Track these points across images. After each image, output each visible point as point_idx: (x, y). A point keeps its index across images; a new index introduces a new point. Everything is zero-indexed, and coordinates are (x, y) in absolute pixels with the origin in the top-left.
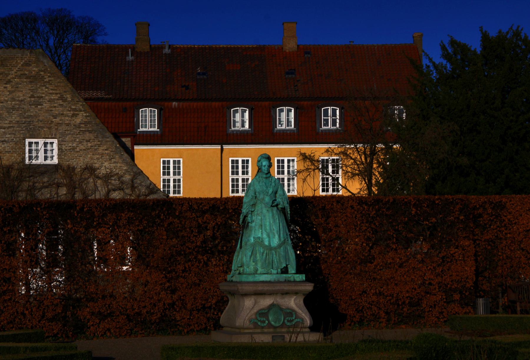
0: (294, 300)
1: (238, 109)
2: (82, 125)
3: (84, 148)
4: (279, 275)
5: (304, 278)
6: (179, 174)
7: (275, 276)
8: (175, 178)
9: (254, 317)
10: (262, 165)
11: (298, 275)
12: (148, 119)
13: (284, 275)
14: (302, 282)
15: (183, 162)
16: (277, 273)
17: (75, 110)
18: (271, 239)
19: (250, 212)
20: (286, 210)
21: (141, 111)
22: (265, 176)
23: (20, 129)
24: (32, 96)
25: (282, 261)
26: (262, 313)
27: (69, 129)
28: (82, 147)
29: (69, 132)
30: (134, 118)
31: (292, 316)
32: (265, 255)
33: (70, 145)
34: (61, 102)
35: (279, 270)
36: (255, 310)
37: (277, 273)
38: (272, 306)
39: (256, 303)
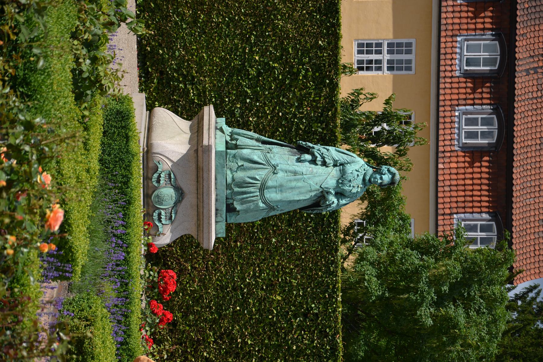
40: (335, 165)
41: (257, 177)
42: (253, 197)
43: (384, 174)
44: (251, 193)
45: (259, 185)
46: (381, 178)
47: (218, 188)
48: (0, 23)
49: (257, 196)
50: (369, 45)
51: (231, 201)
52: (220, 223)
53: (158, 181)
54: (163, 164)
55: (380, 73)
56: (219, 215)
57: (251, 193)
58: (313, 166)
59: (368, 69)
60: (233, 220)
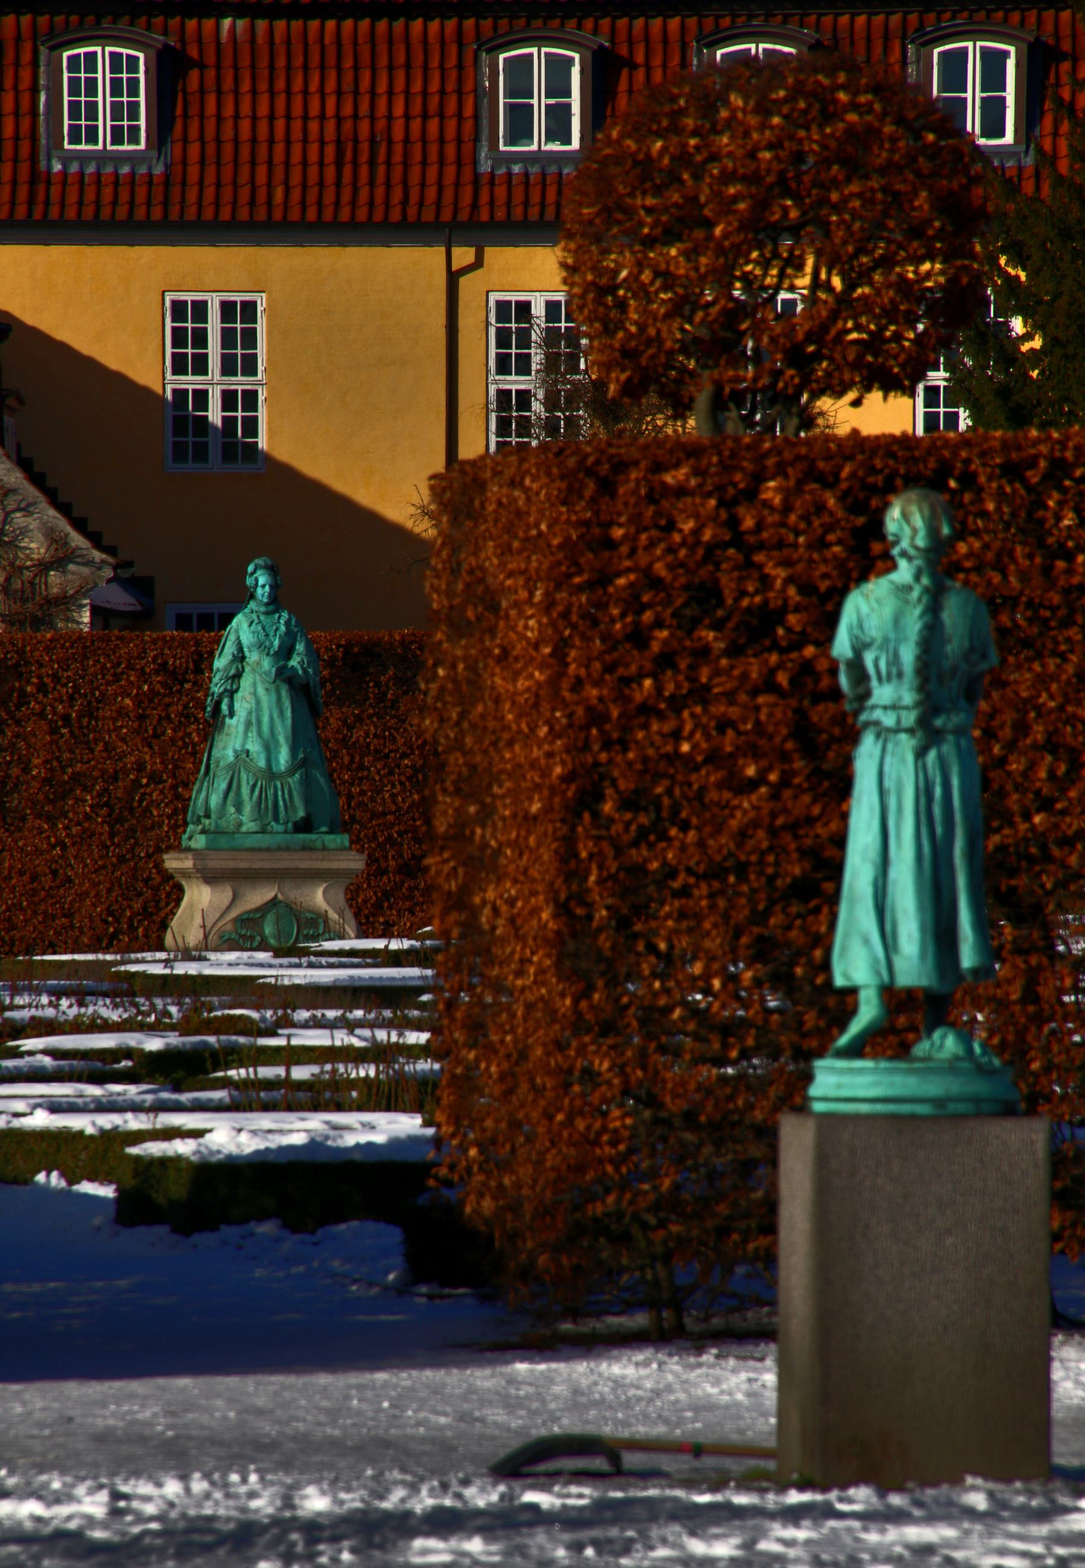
0: (324, 893)
1: (531, 55)
4: (288, 836)
5: (347, 844)
6: (250, 367)
7: (279, 837)
8: (233, 387)
9: (229, 927)
10: (256, 584)
11: (332, 837)
12: (103, 99)
13: (301, 836)
14: (342, 849)
15: (270, 310)
16: (286, 832)
21: (69, 58)
26: (248, 919)
30: (34, 91)
32: (257, 790)
35: (290, 825)
36: (234, 914)
37: (286, 832)
38: (274, 902)
39: (235, 897)
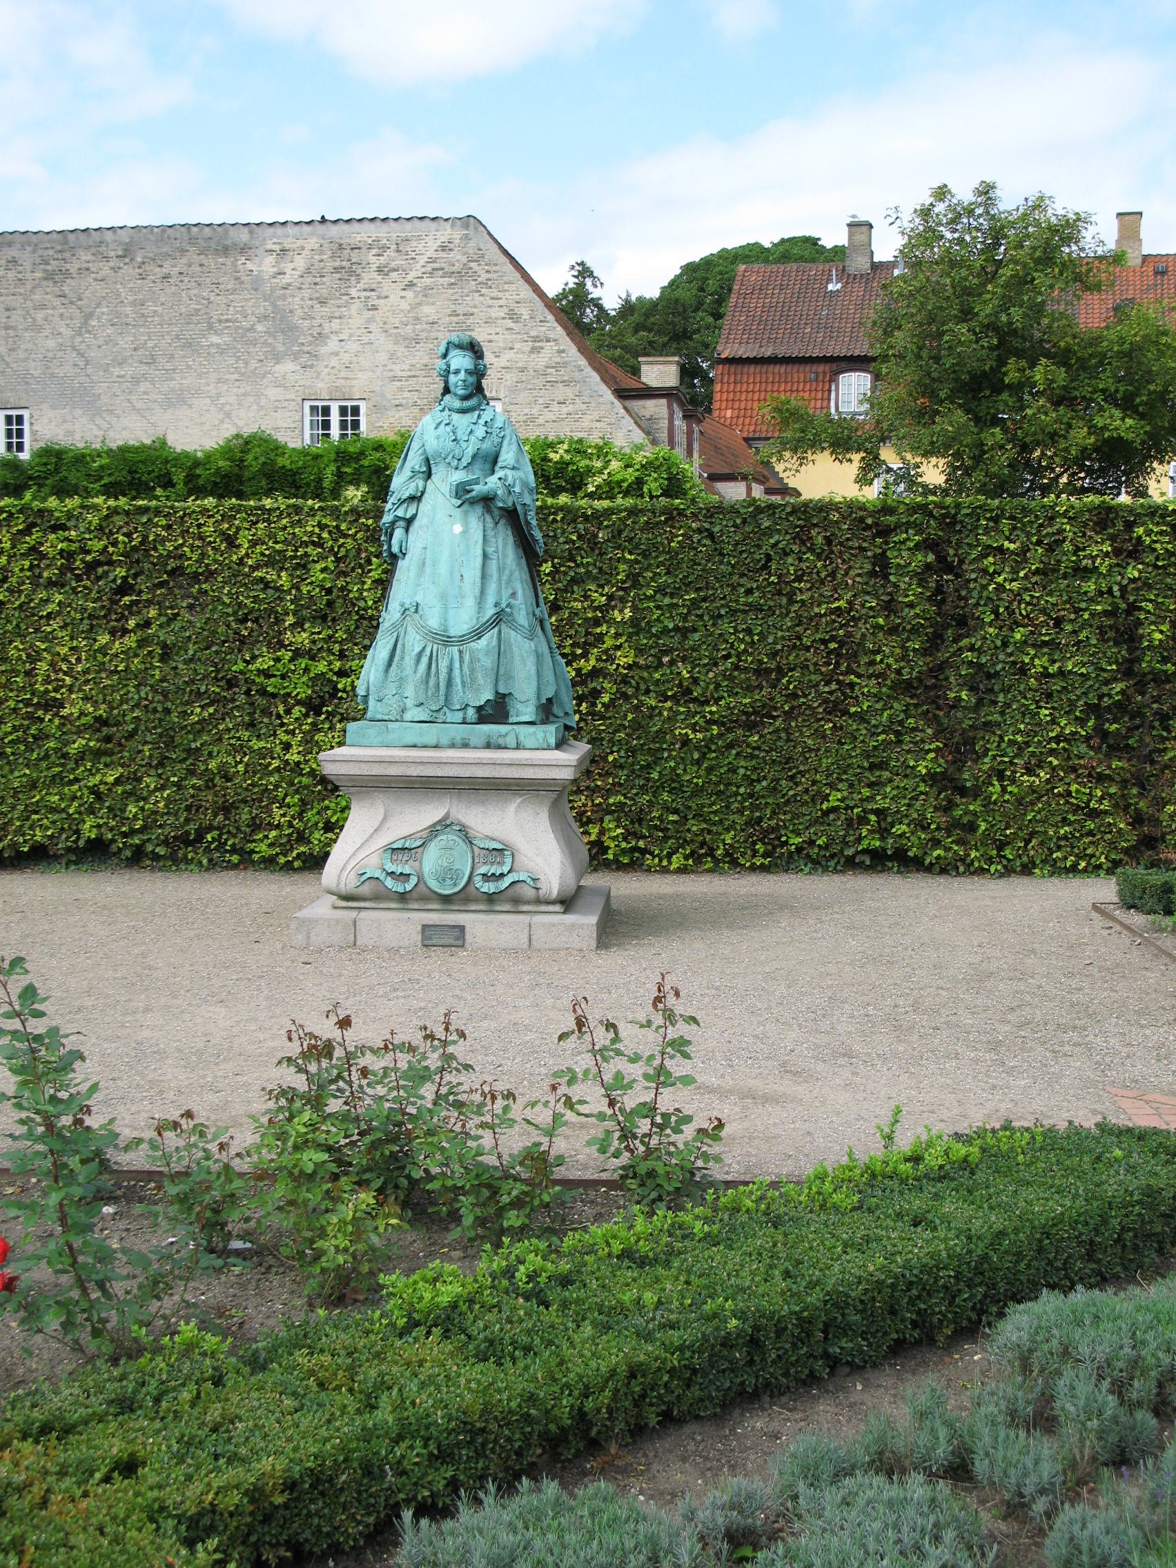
2: (550, 370)
3: (554, 418)
17: (536, 339)
18: (451, 612)
19: (402, 523)
20: (521, 517)
22: (457, 404)
23: (430, 380)
24: (454, 314)
25: (481, 682)
27: (524, 378)
28: (551, 416)
29: (524, 385)
31: (501, 864)
33: (526, 411)
34: (510, 324)
40: (429, 475)
41: (417, 650)
42: (461, 662)
43: (449, 366)
44: (451, 670)
45: (435, 647)
46: (457, 372)
47: (434, 742)
48: (1173, 1224)
49: (461, 652)
50: (9, 434)
51: (471, 713)
52: (522, 738)
53: (404, 877)
54: (366, 866)
55: (362, 411)
56: (501, 741)
57: (451, 670)
58: (416, 524)
59: (20, 433)
60: (525, 709)
